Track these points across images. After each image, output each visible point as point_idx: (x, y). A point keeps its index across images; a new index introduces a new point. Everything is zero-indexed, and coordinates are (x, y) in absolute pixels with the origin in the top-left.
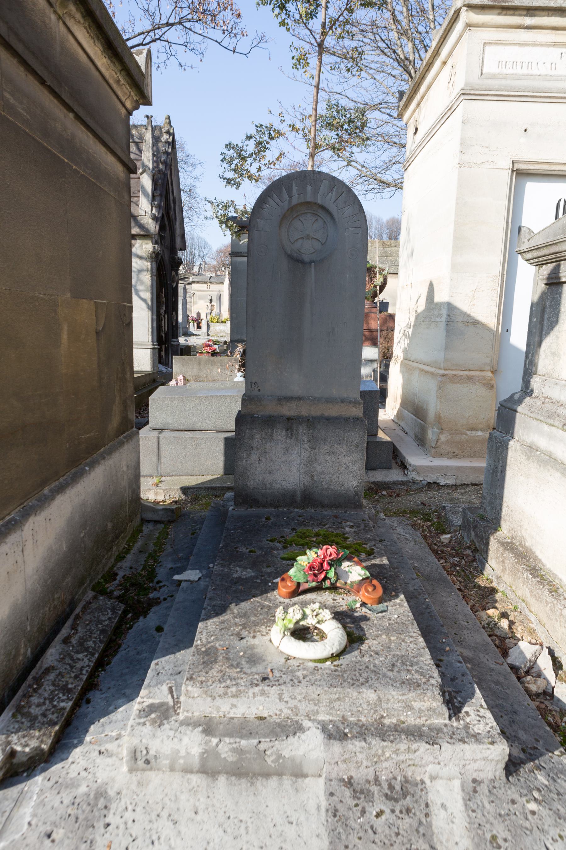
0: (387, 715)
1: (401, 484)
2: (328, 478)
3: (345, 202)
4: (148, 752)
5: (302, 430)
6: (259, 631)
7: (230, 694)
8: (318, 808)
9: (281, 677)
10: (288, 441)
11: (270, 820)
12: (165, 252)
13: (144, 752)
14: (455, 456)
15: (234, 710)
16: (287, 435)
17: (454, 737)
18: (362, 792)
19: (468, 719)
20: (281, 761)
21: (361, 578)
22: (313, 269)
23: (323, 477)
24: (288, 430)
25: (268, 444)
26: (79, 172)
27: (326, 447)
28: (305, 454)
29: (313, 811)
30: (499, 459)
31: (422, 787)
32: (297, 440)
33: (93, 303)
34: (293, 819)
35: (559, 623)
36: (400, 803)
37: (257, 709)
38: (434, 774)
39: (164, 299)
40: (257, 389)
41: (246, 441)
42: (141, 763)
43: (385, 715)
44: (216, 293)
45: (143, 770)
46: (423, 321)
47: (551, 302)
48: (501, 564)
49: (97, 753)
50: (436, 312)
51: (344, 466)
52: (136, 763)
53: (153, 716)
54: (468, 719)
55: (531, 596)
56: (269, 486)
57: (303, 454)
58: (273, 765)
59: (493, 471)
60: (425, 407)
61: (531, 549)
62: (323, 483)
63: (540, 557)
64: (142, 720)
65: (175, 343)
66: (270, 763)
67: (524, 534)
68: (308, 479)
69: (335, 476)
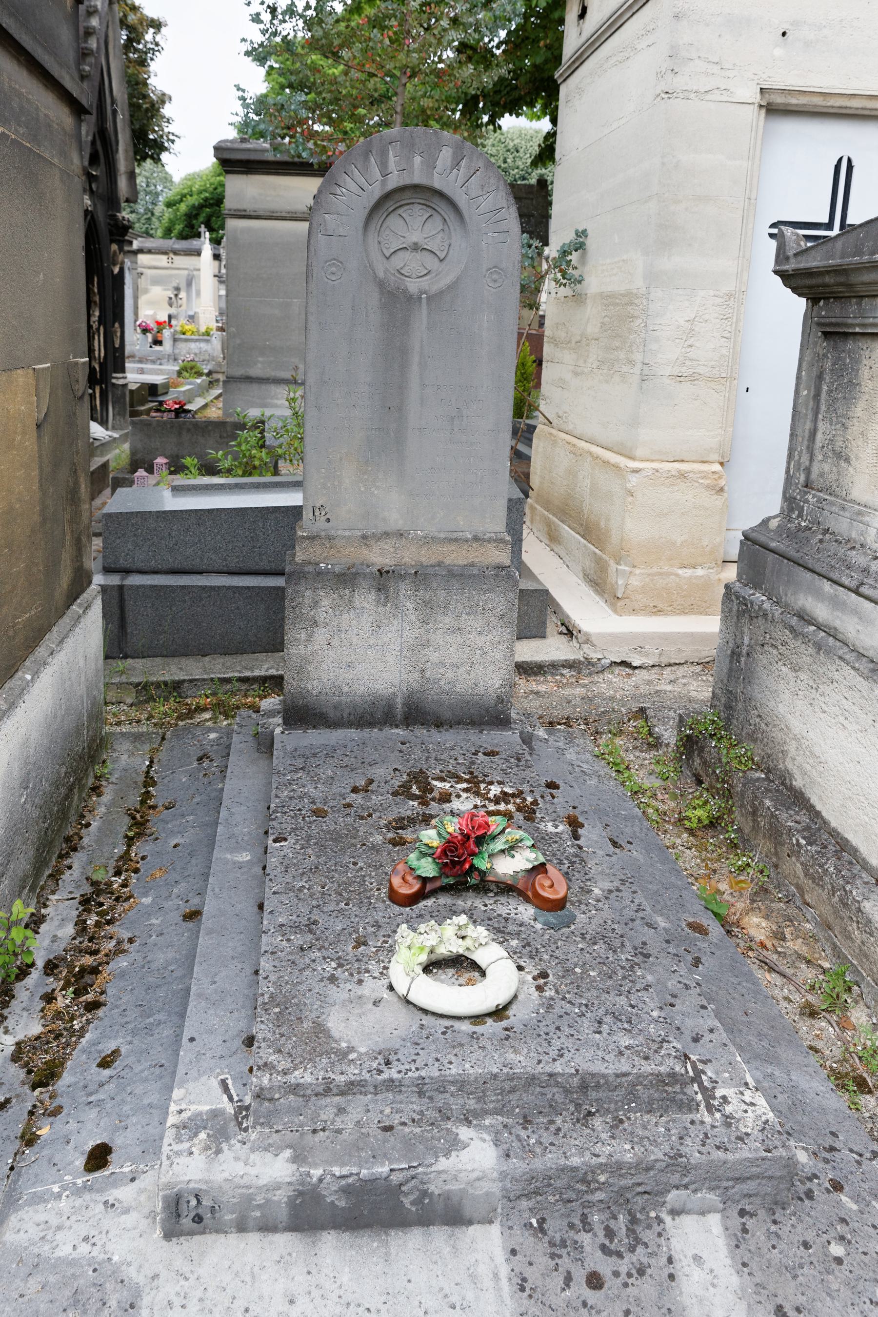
0: (598, 1111)
1: (563, 666)
2: (450, 674)
3: (483, 186)
4: (199, 1202)
5: (404, 589)
6: (367, 971)
7: (335, 1091)
8: (496, 1276)
9: (418, 1054)
10: (381, 609)
11: (417, 1303)
12: (99, 206)
13: (194, 1202)
14: (657, 611)
15: (342, 1117)
16: (378, 601)
17: (708, 1141)
18: (563, 1244)
19: (728, 1109)
20: (427, 1201)
21: (531, 866)
22: (424, 311)
23: (441, 671)
24: (379, 590)
25: (345, 616)
26: (8, 136)
27: (447, 620)
28: (410, 635)
29: (487, 1282)
30: (742, 633)
31: (658, 1229)
33: (31, 371)
34: (454, 1299)
35: (855, 925)
36: (626, 1260)
37: (381, 1112)
38: (677, 1206)
40: (323, 519)
42: (186, 1222)
43: (593, 1110)
45: (191, 1233)
46: (598, 368)
47: (834, 364)
48: (750, 818)
49: (101, 1206)
50: (622, 355)
51: (478, 652)
52: (178, 1222)
53: (203, 1135)
54: (728, 1109)
55: (806, 875)
56: (346, 689)
57: (406, 633)
58: (414, 1209)
59: (733, 653)
60: (602, 524)
61: (802, 794)
62: (442, 683)
63: (818, 808)
64: (186, 1145)
65: (121, 382)
66: (408, 1206)
67: (790, 766)
68: (416, 675)
69: (462, 670)
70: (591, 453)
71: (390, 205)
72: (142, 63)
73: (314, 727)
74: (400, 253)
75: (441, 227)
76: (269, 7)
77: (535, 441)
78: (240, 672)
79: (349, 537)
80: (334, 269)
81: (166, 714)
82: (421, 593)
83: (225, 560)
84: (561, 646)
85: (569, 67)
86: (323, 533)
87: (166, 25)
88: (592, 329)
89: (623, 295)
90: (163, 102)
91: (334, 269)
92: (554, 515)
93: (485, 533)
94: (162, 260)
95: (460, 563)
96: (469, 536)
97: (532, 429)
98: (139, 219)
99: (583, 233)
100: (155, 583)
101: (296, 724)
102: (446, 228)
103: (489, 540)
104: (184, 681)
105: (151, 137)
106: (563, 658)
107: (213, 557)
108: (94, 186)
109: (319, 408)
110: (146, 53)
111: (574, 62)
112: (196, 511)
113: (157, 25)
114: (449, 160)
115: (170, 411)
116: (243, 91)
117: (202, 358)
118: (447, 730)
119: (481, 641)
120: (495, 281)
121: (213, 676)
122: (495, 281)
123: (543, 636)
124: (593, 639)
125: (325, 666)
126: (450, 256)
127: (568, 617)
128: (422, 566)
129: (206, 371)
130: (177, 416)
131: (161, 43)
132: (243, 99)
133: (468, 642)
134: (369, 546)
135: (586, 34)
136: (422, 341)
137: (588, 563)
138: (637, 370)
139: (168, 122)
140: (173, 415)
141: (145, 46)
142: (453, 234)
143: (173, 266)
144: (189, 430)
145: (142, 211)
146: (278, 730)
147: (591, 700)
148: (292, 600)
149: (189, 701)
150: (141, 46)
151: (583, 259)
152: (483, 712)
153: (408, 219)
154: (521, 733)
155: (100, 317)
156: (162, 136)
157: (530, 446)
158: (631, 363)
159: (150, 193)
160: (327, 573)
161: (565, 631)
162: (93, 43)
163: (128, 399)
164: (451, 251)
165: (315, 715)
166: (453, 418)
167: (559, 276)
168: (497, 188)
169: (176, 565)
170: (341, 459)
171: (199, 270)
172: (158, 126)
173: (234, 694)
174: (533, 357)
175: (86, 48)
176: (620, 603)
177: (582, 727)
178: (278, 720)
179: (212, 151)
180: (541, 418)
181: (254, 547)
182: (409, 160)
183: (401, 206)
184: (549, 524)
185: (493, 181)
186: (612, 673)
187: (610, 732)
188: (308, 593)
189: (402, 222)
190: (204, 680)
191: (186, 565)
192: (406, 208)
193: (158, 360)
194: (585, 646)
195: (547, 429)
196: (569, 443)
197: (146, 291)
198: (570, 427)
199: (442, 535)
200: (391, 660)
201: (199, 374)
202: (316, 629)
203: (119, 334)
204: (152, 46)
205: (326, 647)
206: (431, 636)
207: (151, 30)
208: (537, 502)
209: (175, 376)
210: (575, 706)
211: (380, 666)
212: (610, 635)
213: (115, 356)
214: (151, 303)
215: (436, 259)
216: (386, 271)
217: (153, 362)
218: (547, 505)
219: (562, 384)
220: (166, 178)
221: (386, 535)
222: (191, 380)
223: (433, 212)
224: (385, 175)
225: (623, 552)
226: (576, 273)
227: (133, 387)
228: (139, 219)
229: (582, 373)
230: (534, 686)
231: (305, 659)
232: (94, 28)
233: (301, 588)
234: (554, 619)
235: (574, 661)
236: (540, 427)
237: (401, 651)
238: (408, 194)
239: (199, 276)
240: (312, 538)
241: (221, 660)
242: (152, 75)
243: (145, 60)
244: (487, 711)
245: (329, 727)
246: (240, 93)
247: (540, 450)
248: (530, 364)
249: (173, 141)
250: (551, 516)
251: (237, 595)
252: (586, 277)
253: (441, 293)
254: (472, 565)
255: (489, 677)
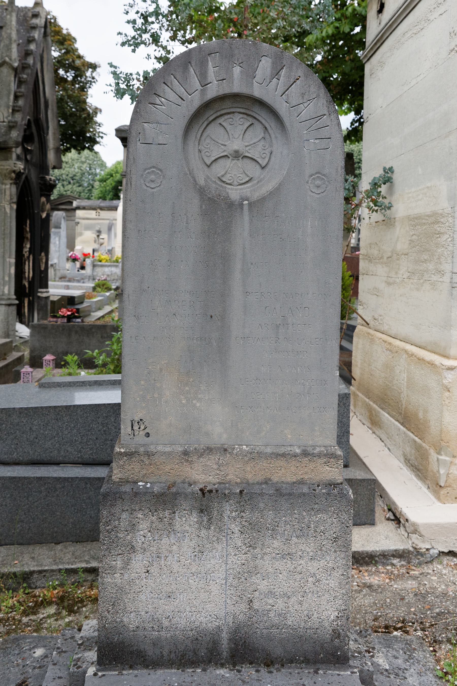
1: (394, 556)
2: (280, 605)
3: (303, 95)
10: (204, 532)
16: (200, 523)
23: (271, 601)
24: (202, 511)
25: (165, 540)
27: (276, 544)
32: (221, 530)
39: (29, 235)
40: (142, 433)
41: (121, 535)
44: (108, 222)
46: (409, 278)
50: (431, 266)
51: (310, 579)
56: (166, 623)
57: (232, 559)
60: (421, 415)
62: (272, 615)
65: (44, 295)
68: (243, 607)
69: (293, 599)
70: (406, 351)
71: (210, 114)
72: (83, 89)
73: (131, 667)
74: (221, 161)
75: (262, 135)
76: (142, 14)
77: (355, 339)
78: (87, 562)
79: (170, 453)
80: (153, 177)
81: (12, 608)
82: (247, 514)
83: (80, 452)
84: (391, 535)
85: (372, 49)
86: (142, 449)
87: (99, 67)
88: (402, 246)
89: (429, 216)
90: (96, 113)
91: (153, 177)
92: (374, 402)
93: (314, 447)
94: (92, 214)
95: (289, 480)
96: (298, 451)
97: (352, 328)
98: (84, 190)
99: (391, 170)
100: (15, 474)
101: (110, 663)
102: (267, 136)
103: (319, 455)
104: (32, 573)
105: (88, 135)
106: (393, 548)
107: (69, 449)
108: (28, 157)
109: (137, 317)
110: (86, 83)
111: (376, 44)
112: (55, 407)
113: (94, 67)
114: (269, 69)
115: (63, 317)
116: (115, 67)
117: (112, 278)
118: (278, 670)
119: (313, 567)
120: (318, 187)
121: (61, 567)
122: (318, 187)
123: (373, 524)
124: (421, 529)
125: (143, 597)
126: (271, 163)
127: (394, 503)
128: (248, 483)
129: (114, 287)
130: (69, 321)
131: (96, 77)
132: (114, 73)
133: (299, 569)
134: (191, 462)
135: (383, 24)
136: (244, 248)
137: (408, 449)
138: (447, 278)
139: (99, 126)
140: (65, 320)
141: (85, 79)
142: (274, 141)
143: (100, 217)
144: (76, 332)
145: (86, 185)
146: (91, 670)
147: (424, 596)
148: (108, 523)
149: (37, 592)
150: (83, 80)
151: (391, 190)
152: (318, 648)
153: (228, 127)
154: (361, 672)
155: (30, 248)
156: (95, 135)
157: (351, 342)
158: (441, 273)
159: (92, 174)
160: (145, 494)
161: (392, 517)
162: (30, 61)
163: (49, 308)
164: (273, 158)
165: (132, 653)
166: (278, 327)
167: (372, 204)
168: (318, 96)
169: (36, 457)
170: (161, 370)
171: (116, 220)
172: (92, 128)
173: (79, 585)
174: (349, 273)
175: (25, 64)
176: (443, 492)
177: (419, 633)
178: (92, 655)
179: (114, 132)
180: (360, 320)
181: (106, 440)
182: (229, 71)
183: (221, 115)
184: (370, 410)
185: (312, 89)
186: (441, 563)
187: (449, 641)
188: (124, 516)
189: (222, 130)
190: (52, 571)
191: (45, 457)
192: (226, 117)
193: (82, 280)
194: (414, 536)
195: (365, 329)
196: (385, 342)
197: (81, 234)
198: (385, 328)
199: (269, 450)
200: (215, 589)
201: (109, 289)
202: (133, 556)
203: (44, 261)
204: (90, 79)
205: (144, 575)
206: (259, 562)
207: (90, 70)
208: (358, 389)
209: (91, 291)
210: (409, 605)
211: (203, 596)
212: (437, 525)
213: (40, 276)
214: (84, 242)
215: (258, 167)
216: (207, 178)
217: (78, 281)
218: (368, 393)
219: (376, 292)
220: (102, 164)
221: (210, 450)
222: (102, 293)
223: (254, 121)
224: (204, 85)
225: (443, 444)
226: (386, 202)
227: (56, 299)
228: (84, 190)
229: (394, 283)
230: (367, 579)
231: (121, 588)
232: (32, 50)
233: (117, 510)
234: (381, 503)
235: (404, 551)
236: (359, 328)
237: (226, 579)
238: (228, 103)
239: (116, 224)
240: (130, 455)
241: (72, 548)
242: (89, 96)
243: (85, 88)
244: (322, 648)
245: (147, 667)
246: (113, 69)
247: (360, 346)
248: (347, 278)
249: (102, 137)
250: (371, 403)
251: (88, 485)
252: (393, 204)
253: (263, 200)
254: (301, 482)
255: (323, 608)
